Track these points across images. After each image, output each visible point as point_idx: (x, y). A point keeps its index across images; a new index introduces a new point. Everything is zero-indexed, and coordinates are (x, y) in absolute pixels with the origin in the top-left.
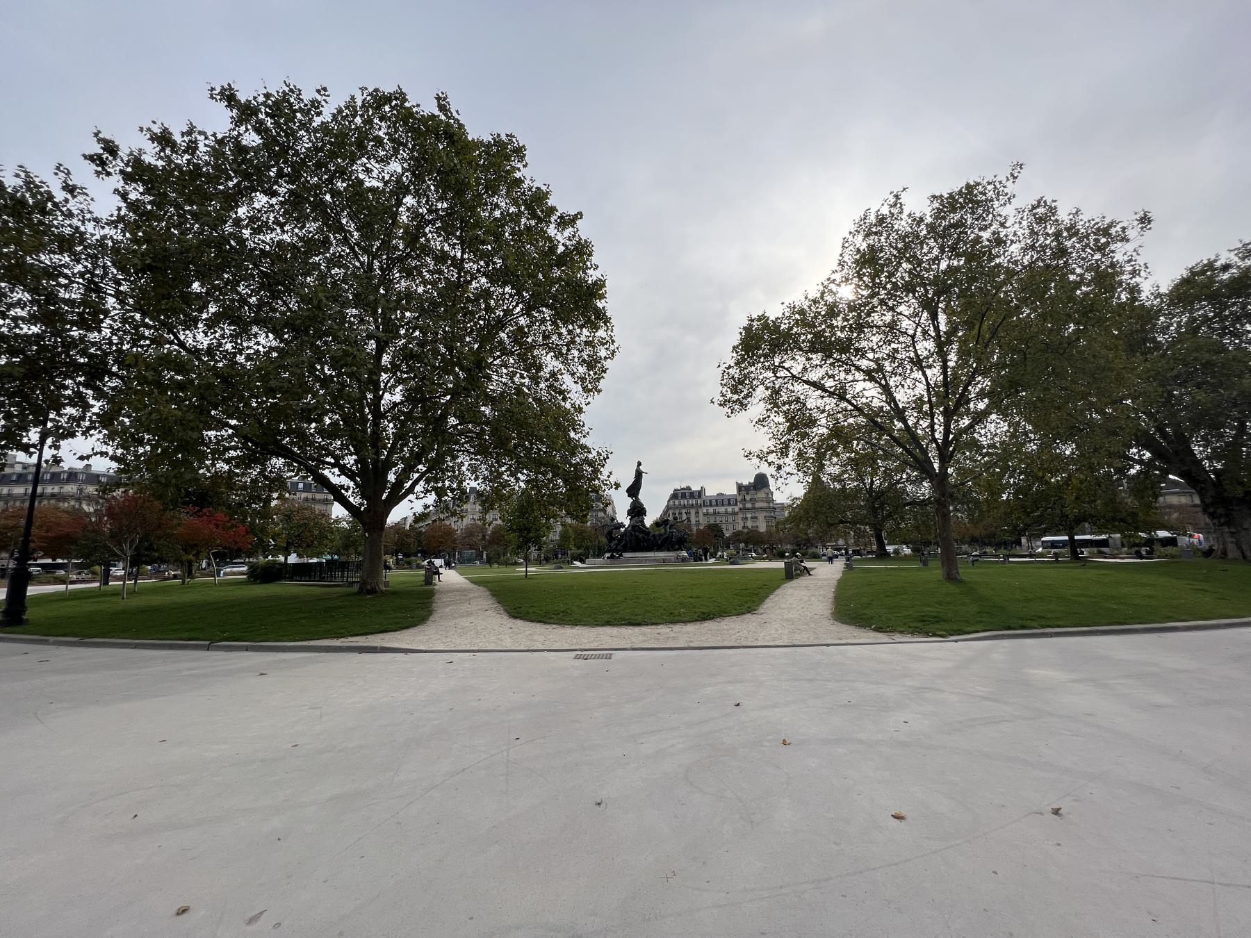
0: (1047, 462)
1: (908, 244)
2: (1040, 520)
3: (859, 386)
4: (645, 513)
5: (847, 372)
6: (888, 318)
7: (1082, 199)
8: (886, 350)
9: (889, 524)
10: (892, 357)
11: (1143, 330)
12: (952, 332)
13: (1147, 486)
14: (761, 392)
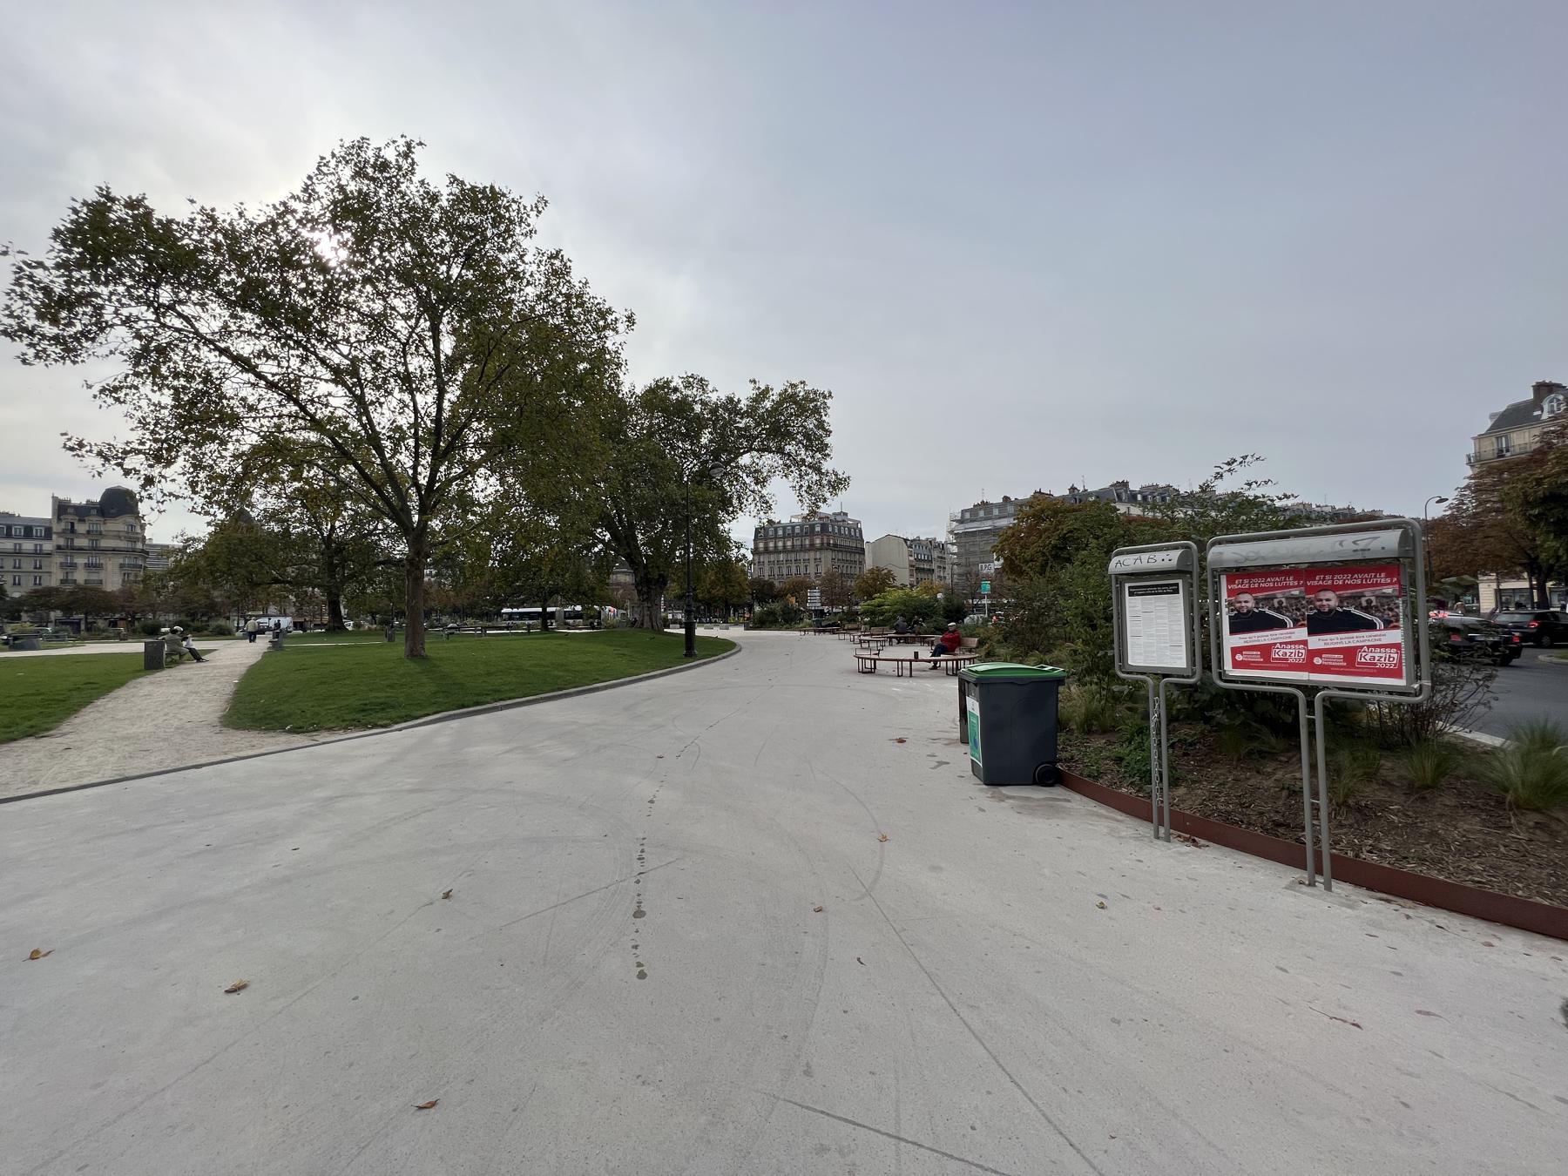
0: (528, 534)
1: (415, 222)
2: (519, 591)
3: (323, 388)
4: (889, 575)
5: (304, 360)
6: (378, 306)
7: (600, 276)
8: (369, 350)
9: (350, 588)
10: (375, 359)
11: (618, 422)
12: (455, 361)
13: (604, 565)
14: (119, 336)
